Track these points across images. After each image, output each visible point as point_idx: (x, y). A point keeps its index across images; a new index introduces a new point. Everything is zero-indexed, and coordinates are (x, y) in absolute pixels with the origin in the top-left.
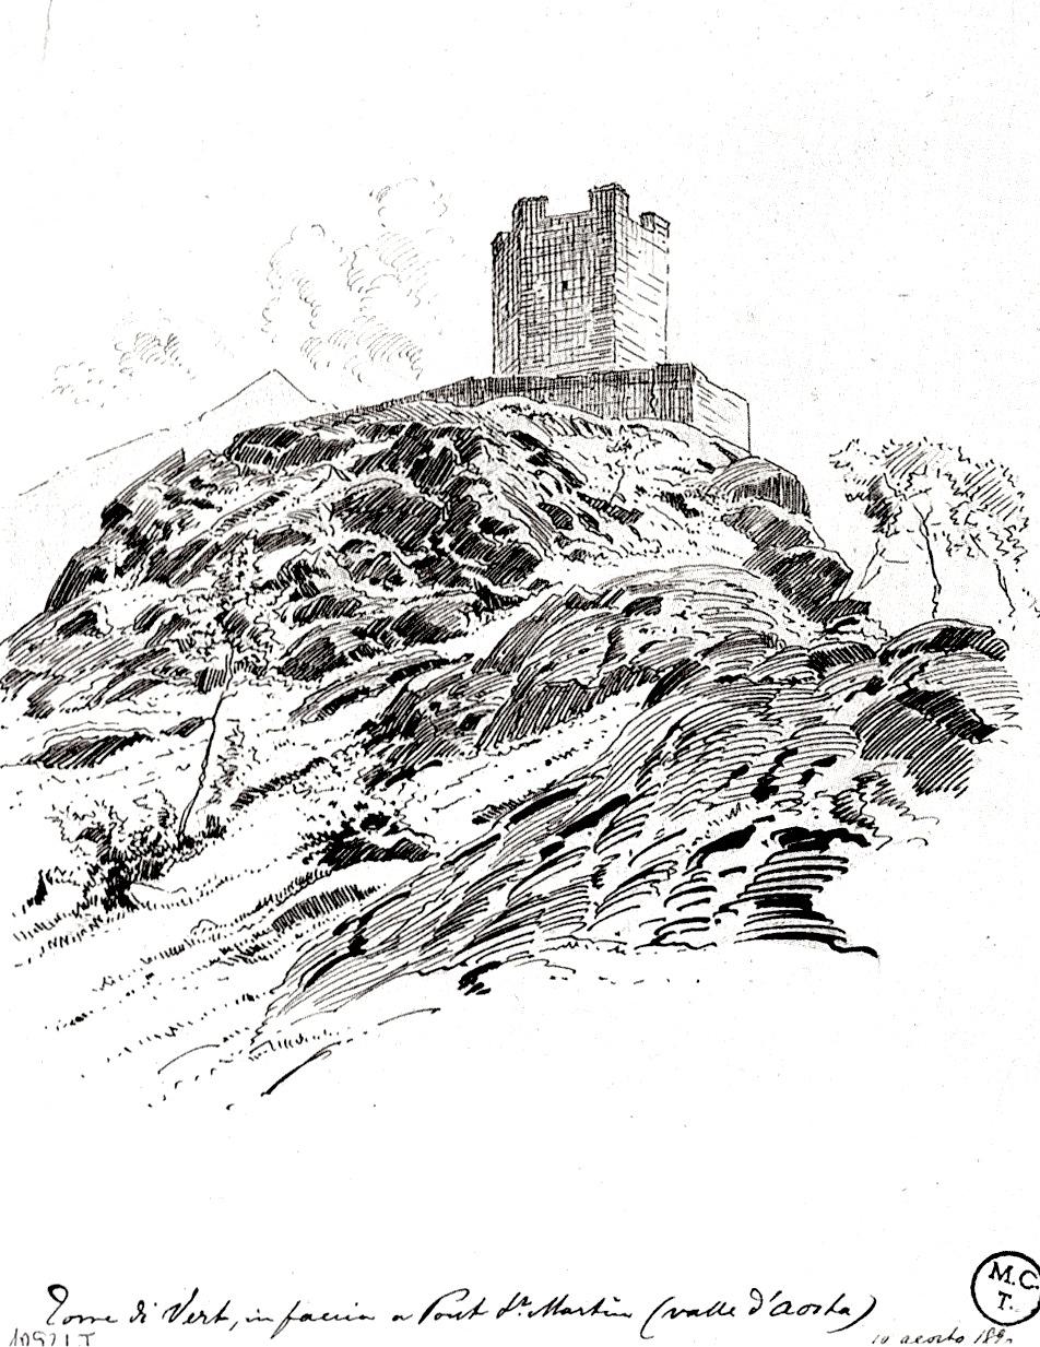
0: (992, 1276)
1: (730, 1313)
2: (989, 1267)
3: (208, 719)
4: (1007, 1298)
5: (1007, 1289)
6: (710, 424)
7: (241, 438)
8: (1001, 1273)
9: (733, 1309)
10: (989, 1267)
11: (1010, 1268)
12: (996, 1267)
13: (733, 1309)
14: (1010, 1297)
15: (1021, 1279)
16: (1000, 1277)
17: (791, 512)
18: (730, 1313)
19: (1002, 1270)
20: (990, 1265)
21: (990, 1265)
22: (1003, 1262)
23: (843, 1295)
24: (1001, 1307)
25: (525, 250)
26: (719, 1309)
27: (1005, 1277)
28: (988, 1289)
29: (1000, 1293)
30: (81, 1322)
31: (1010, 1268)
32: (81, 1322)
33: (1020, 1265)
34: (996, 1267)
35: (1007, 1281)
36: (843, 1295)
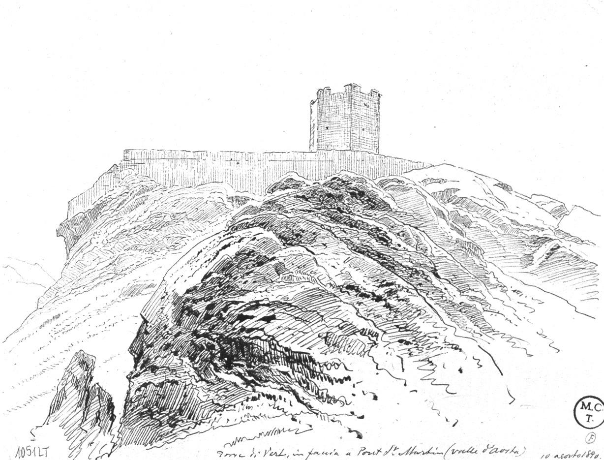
0: (582, 408)
1: (475, 452)
2: (580, 404)
3: (265, 332)
4: (590, 417)
5: (590, 412)
6: (549, 276)
7: (337, 182)
8: (586, 406)
9: (476, 451)
10: (580, 404)
11: (589, 404)
12: (583, 404)
13: (476, 451)
14: (592, 416)
15: (595, 408)
16: (586, 408)
17: (542, 231)
18: (475, 452)
19: (586, 404)
20: (581, 403)
21: (581, 403)
22: (586, 401)
23: (502, 374)
24: (588, 421)
25: (207, 324)
26: (471, 451)
27: (588, 408)
28: (582, 414)
29: (587, 415)
30: (279, 406)
31: (589, 404)
32: (279, 406)
33: (594, 402)
34: (583, 404)
35: (589, 409)
36: (502, 374)
